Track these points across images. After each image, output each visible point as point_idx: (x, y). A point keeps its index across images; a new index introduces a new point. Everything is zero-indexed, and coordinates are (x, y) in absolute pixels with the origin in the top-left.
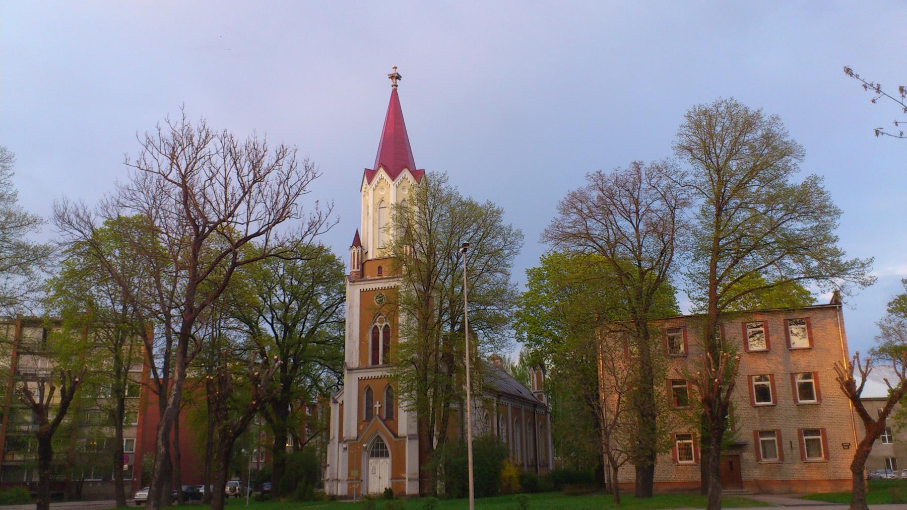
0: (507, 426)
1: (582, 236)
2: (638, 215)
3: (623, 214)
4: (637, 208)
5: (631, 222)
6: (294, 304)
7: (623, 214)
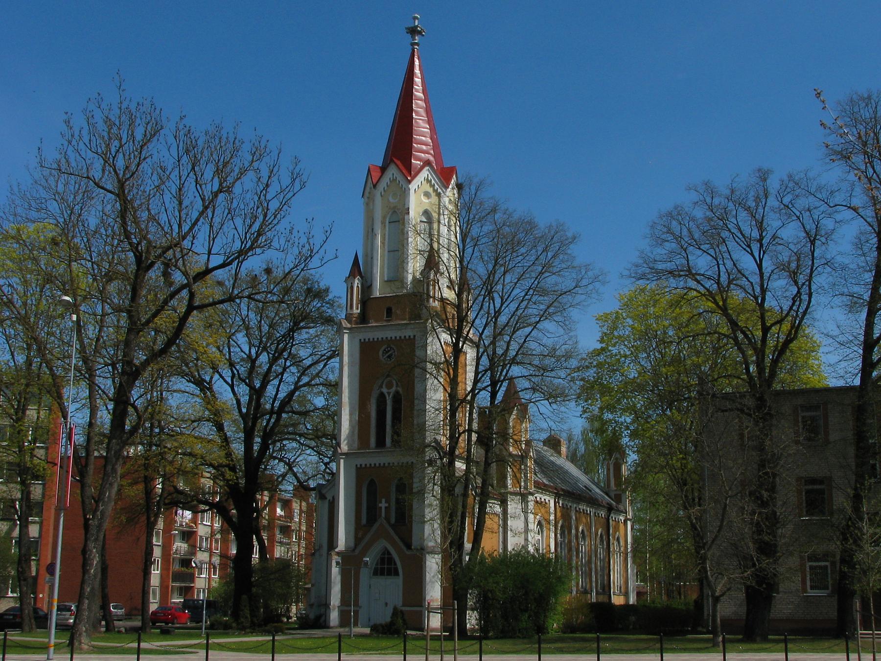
0: (608, 470)
1: (682, 273)
2: (761, 245)
3: (741, 243)
4: (761, 235)
5: (752, 254)
6: (264, 358)
7: (741, 243)
